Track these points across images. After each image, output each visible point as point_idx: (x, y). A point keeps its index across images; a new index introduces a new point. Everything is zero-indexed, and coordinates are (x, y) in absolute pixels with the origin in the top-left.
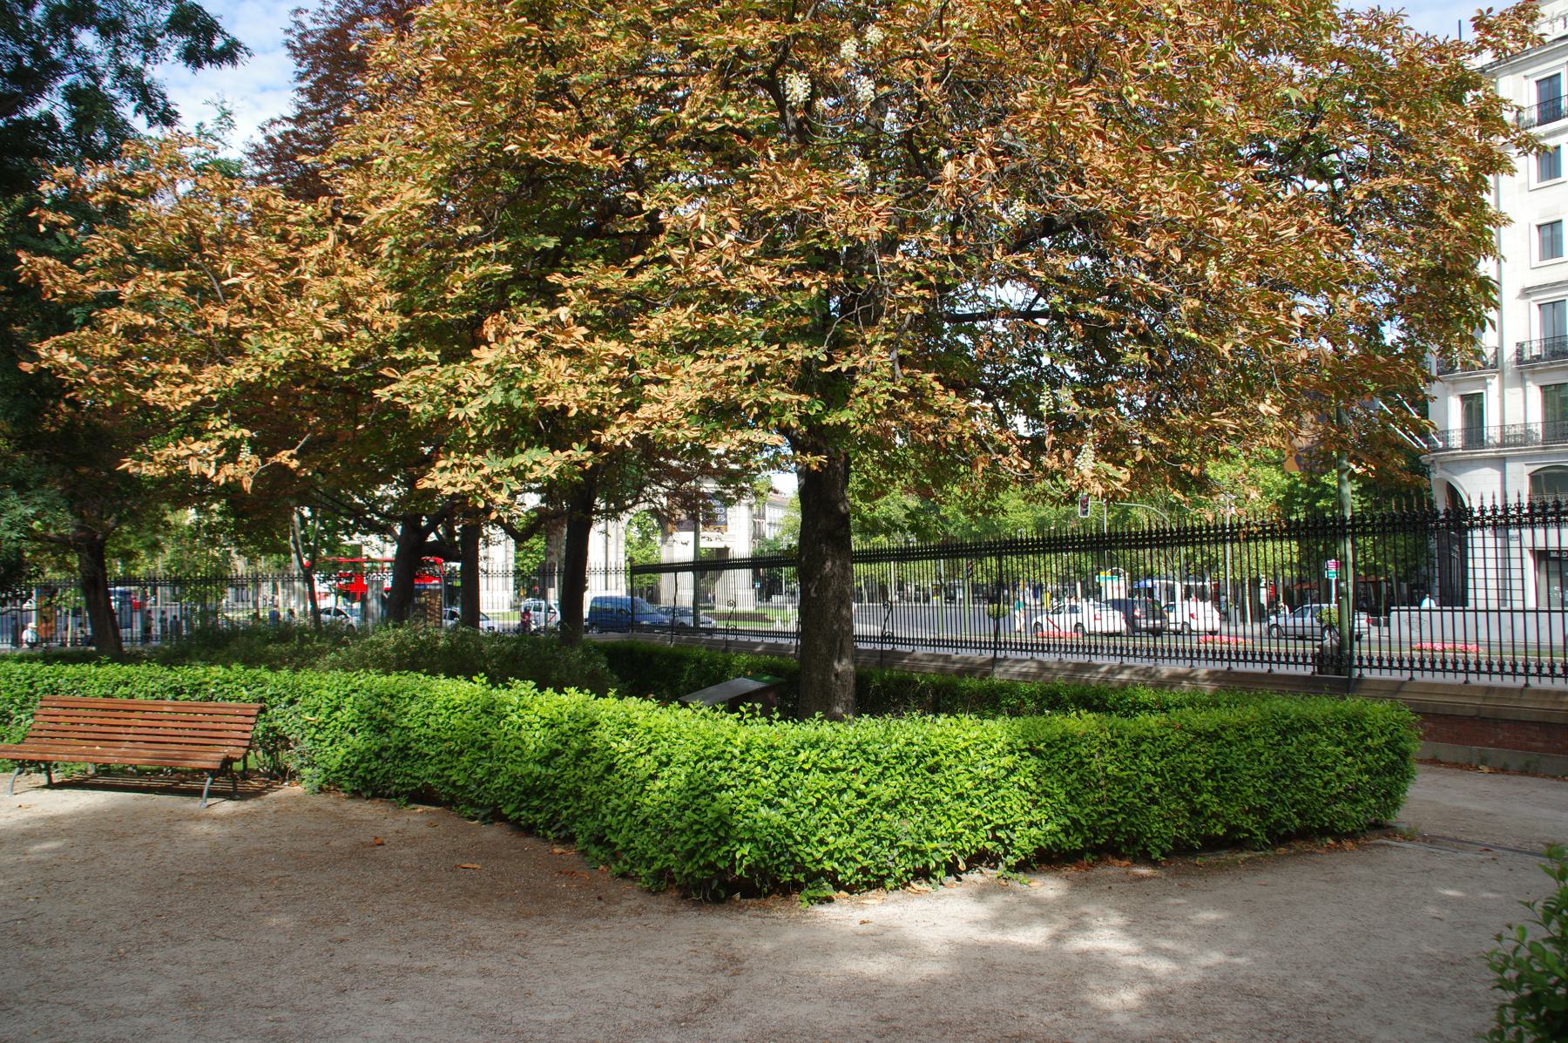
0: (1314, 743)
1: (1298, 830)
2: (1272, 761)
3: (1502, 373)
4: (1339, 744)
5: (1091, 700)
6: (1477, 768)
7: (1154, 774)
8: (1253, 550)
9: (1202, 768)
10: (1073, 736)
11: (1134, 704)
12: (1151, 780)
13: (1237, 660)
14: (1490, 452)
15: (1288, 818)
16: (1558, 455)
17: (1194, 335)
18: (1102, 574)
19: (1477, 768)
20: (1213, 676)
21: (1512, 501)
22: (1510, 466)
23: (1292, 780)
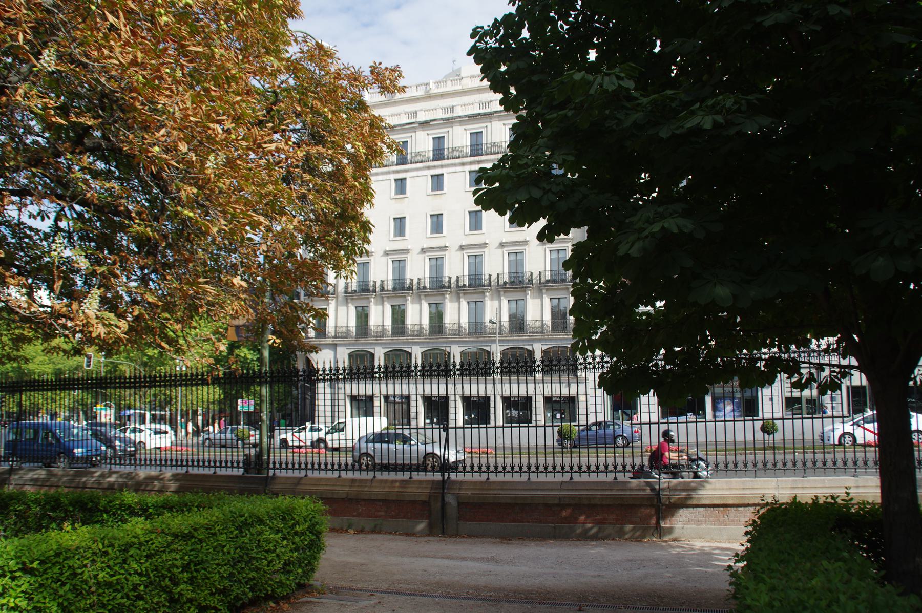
0: (260, 533)
1: (250, 600)
2: (232, 551)
3: (337, 298)
4: (278, 531)
5: (86, 504)
6: (347, 531)
7: (140, 575)
8: (195, 393)
9: (179, 563)
10: (67, 550)
11: (121, 505)
12: (136, 579)
13: (193, 466)
14: (329, 341)
15: (244, 593)
16: (362, 344)
17: (191, 214)
18: (99, 406)
19: (347, 531)
20: (176, 477)
21: (341, 366)
22: (339, 349)
23: (247, 563)
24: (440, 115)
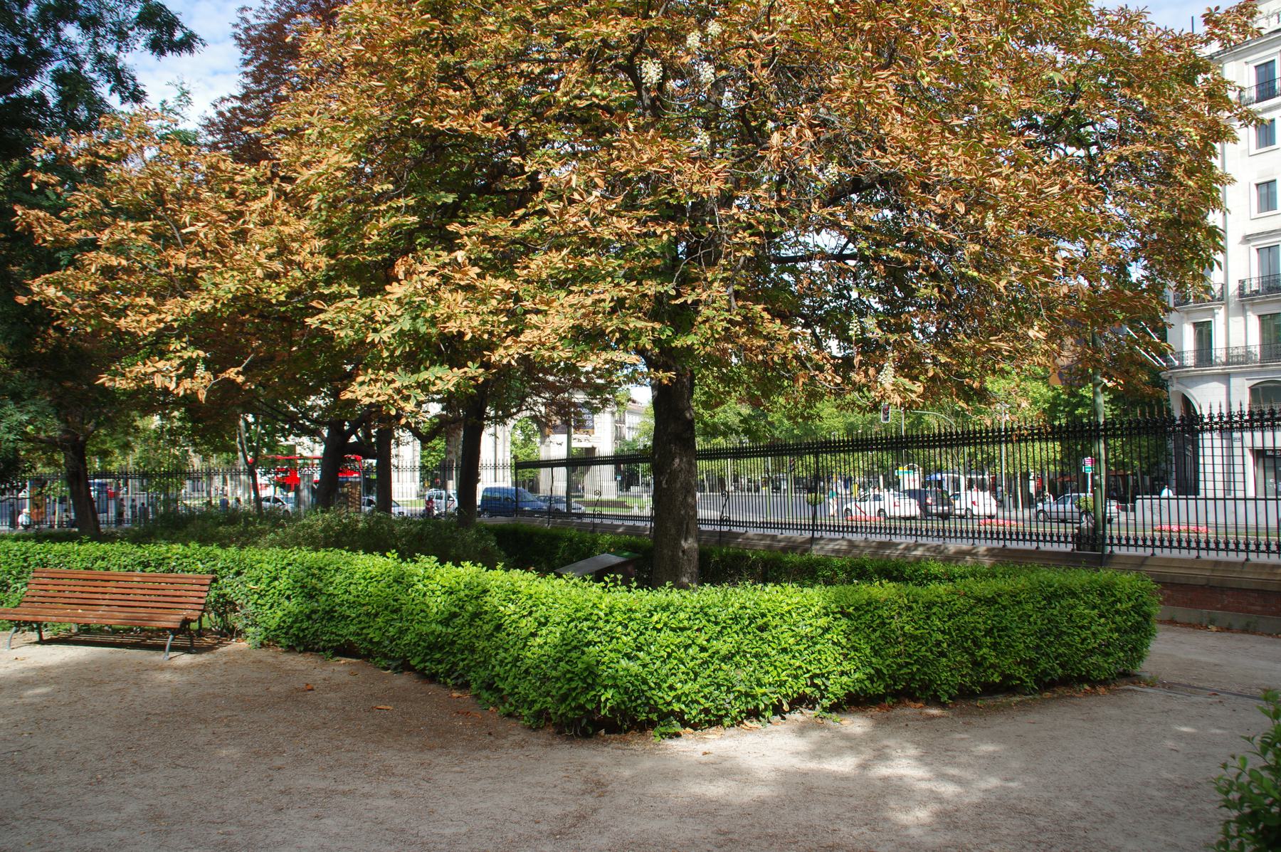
0: (1073, 607)
1: (1060, 678)
2: (1039, 622)
3: (1227, 304)
4: (1094, 607)
5: (891, 572)
6: (1207, 627)
7: (943, 632)
8: (1023, 450)
9: (982, 627)
10: (877, 601)
11: (926, 575)
12: (940, 637)
13: (1011, 539)
14: (1217, 369)
15: (1053, 668)
16: (1273, 371)
17: (976, 274)
18: (900, 469)
19: (1207, 627)
20: (991, 552)
21: (1235, 409)
22: (1233, 381)
23: (1056, 637)
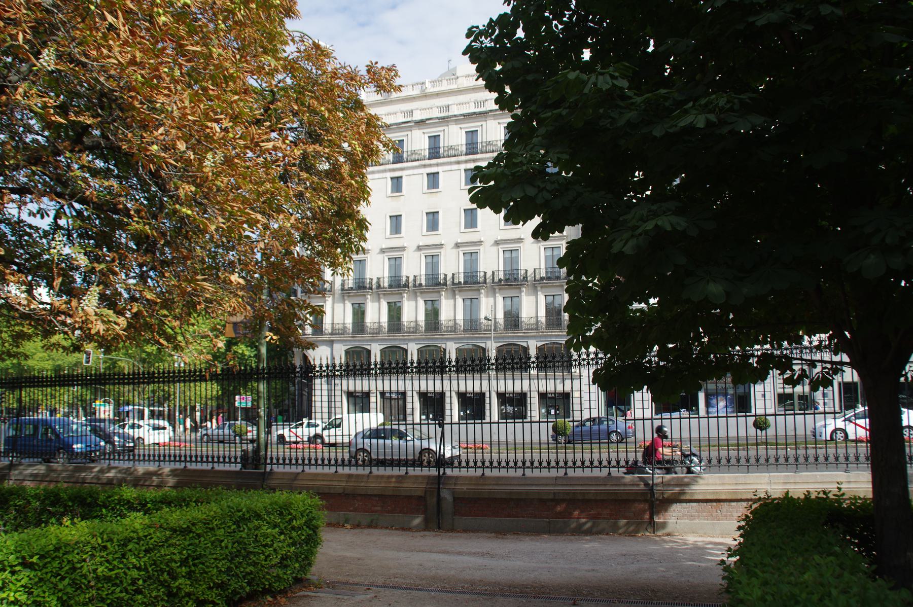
0: (258, 528)
1: (248, 594)
2: (230, 545)
3: (333, 295)
4: (275, 526)
5: (85, 499)
6: (343, 526)
7: (139, 569)
8: (193, 389)
9: (177, 558)
10: (67, 545)
11: (119, 500)
12: (135, 573)
13: (191, 461)
14: (326, 338)
15: (242, 587)
16: (359, 341)
17: (189, 212)
18: (98, 402)
19: (343, 526)
20: (174, 472)
21: (337, 362)
22: (336, 346)
23: (244, 558)
24: (436, 114)
